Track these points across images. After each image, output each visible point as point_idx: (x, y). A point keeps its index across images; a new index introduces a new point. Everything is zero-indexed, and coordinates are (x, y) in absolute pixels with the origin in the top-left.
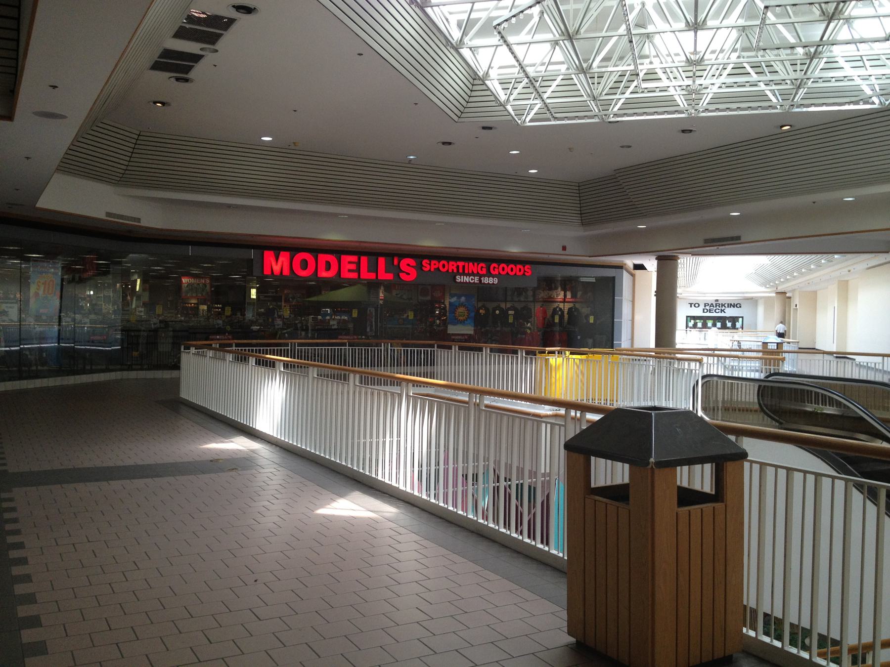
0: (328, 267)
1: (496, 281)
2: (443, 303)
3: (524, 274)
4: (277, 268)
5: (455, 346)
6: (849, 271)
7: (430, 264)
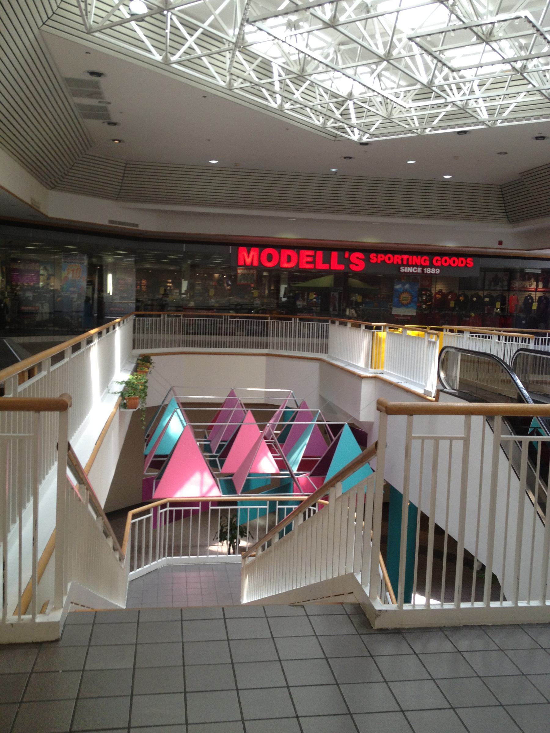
0: (289, 261)
1: (438, 271)
2: (430, 291)
3: (466, 265)
4: (248, 261)
5: (295, 319)
7: (377, 257)
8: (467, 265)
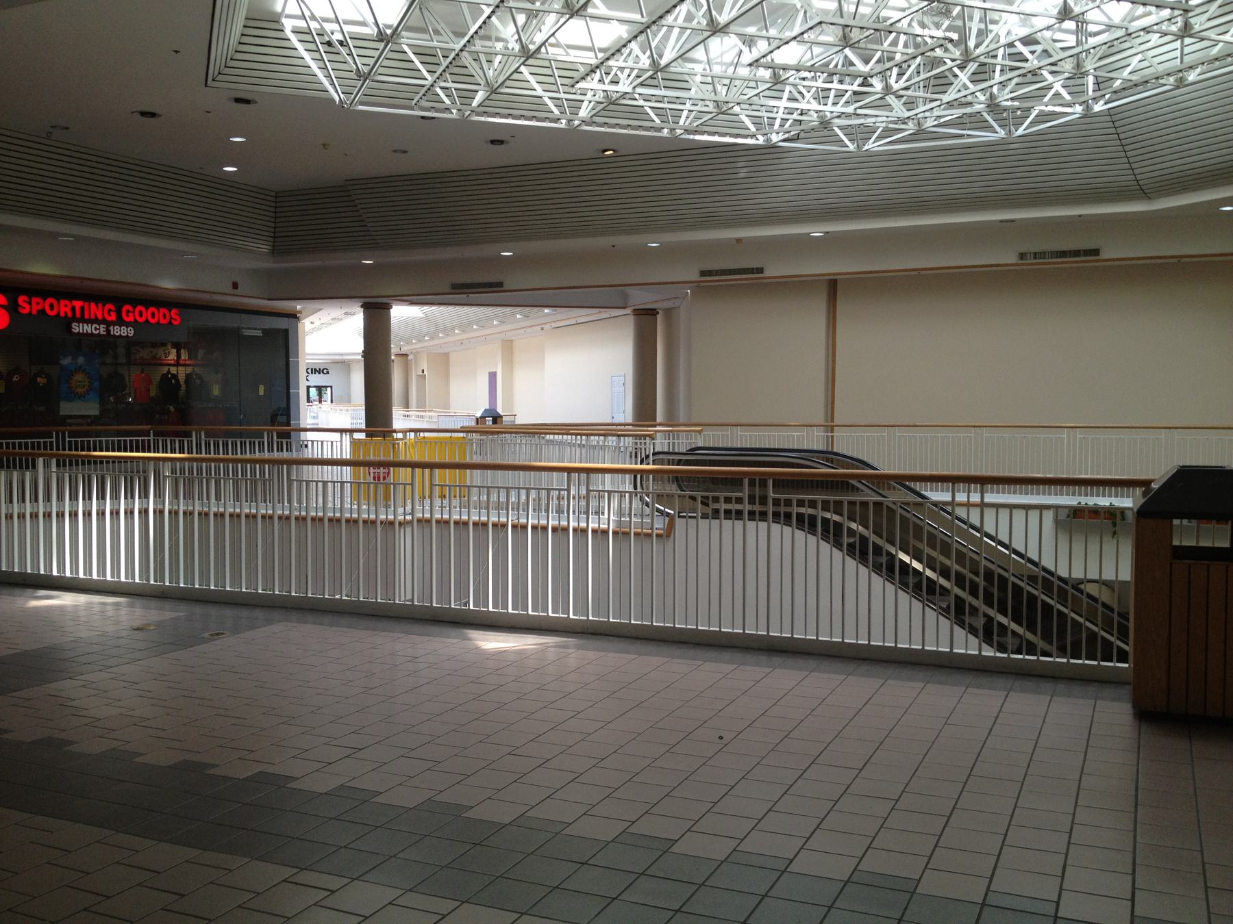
1: (131, 332)
3: (170, 323)
6: (542, 329)
7: (30, 303)
8: (173, 322)
